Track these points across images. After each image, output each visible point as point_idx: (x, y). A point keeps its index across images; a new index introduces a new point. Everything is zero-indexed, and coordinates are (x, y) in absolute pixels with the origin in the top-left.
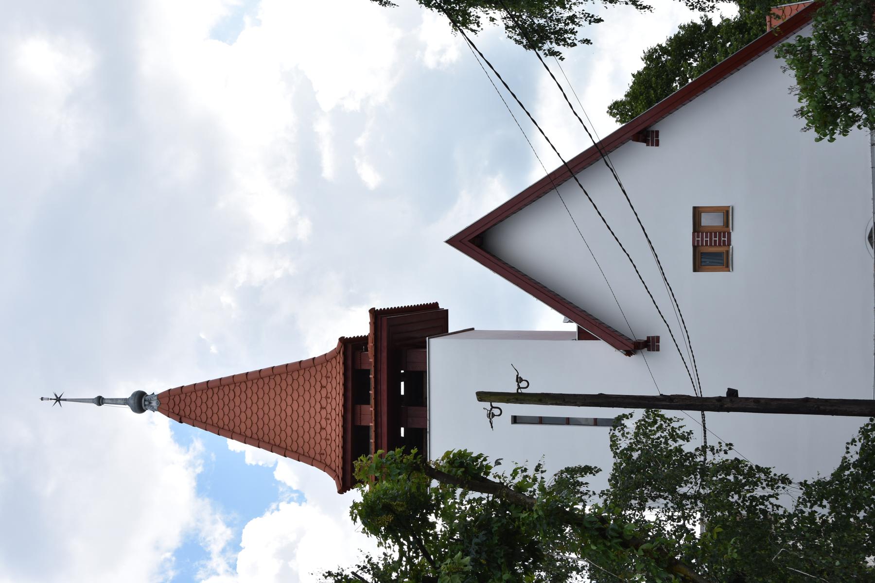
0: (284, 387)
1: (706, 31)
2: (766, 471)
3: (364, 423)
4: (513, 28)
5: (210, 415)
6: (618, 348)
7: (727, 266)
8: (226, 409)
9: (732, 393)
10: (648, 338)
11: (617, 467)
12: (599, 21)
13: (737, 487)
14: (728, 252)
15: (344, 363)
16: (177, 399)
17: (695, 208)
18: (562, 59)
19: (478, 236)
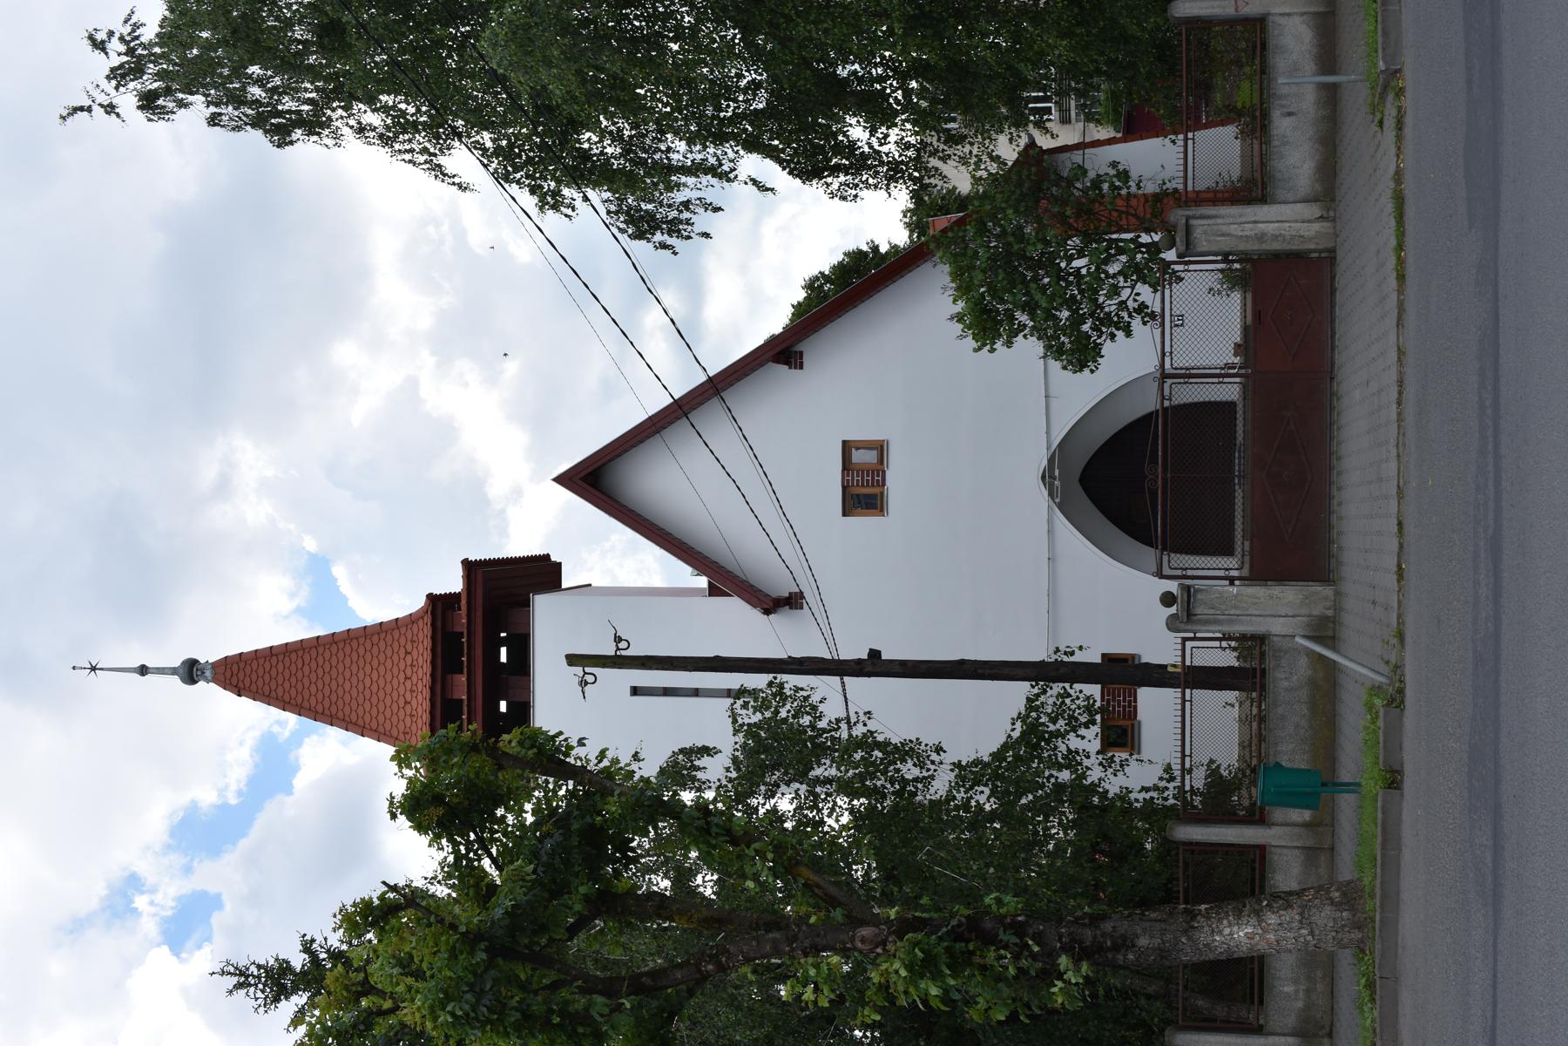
0: (362, 653)
1: (872, 259)
3: (455, 697)
4: (616, 213)
5: (273, 687)
6: (755, 606)
7: (882, 510)
8: (293, 680)
9: (874, 654)
10: (790, 594)
12: (717, 209)
14: (882, 493)
15: (432, 625)
16: (235, 668)
18: (675, 253)
19: (590, 474)
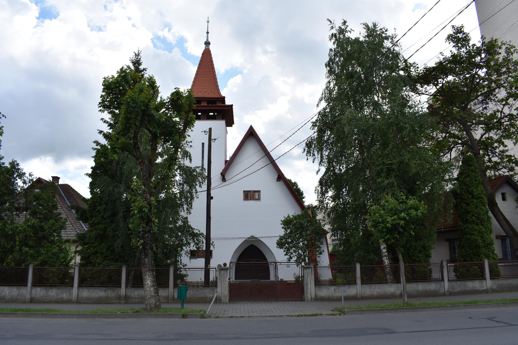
2: (191, 208)
3: (202, 103)
4: (312, 139)
9: (212, 198)
11: (191, 168)
13: (187, 201)
17: (260, 191)
18: (303, 153)
